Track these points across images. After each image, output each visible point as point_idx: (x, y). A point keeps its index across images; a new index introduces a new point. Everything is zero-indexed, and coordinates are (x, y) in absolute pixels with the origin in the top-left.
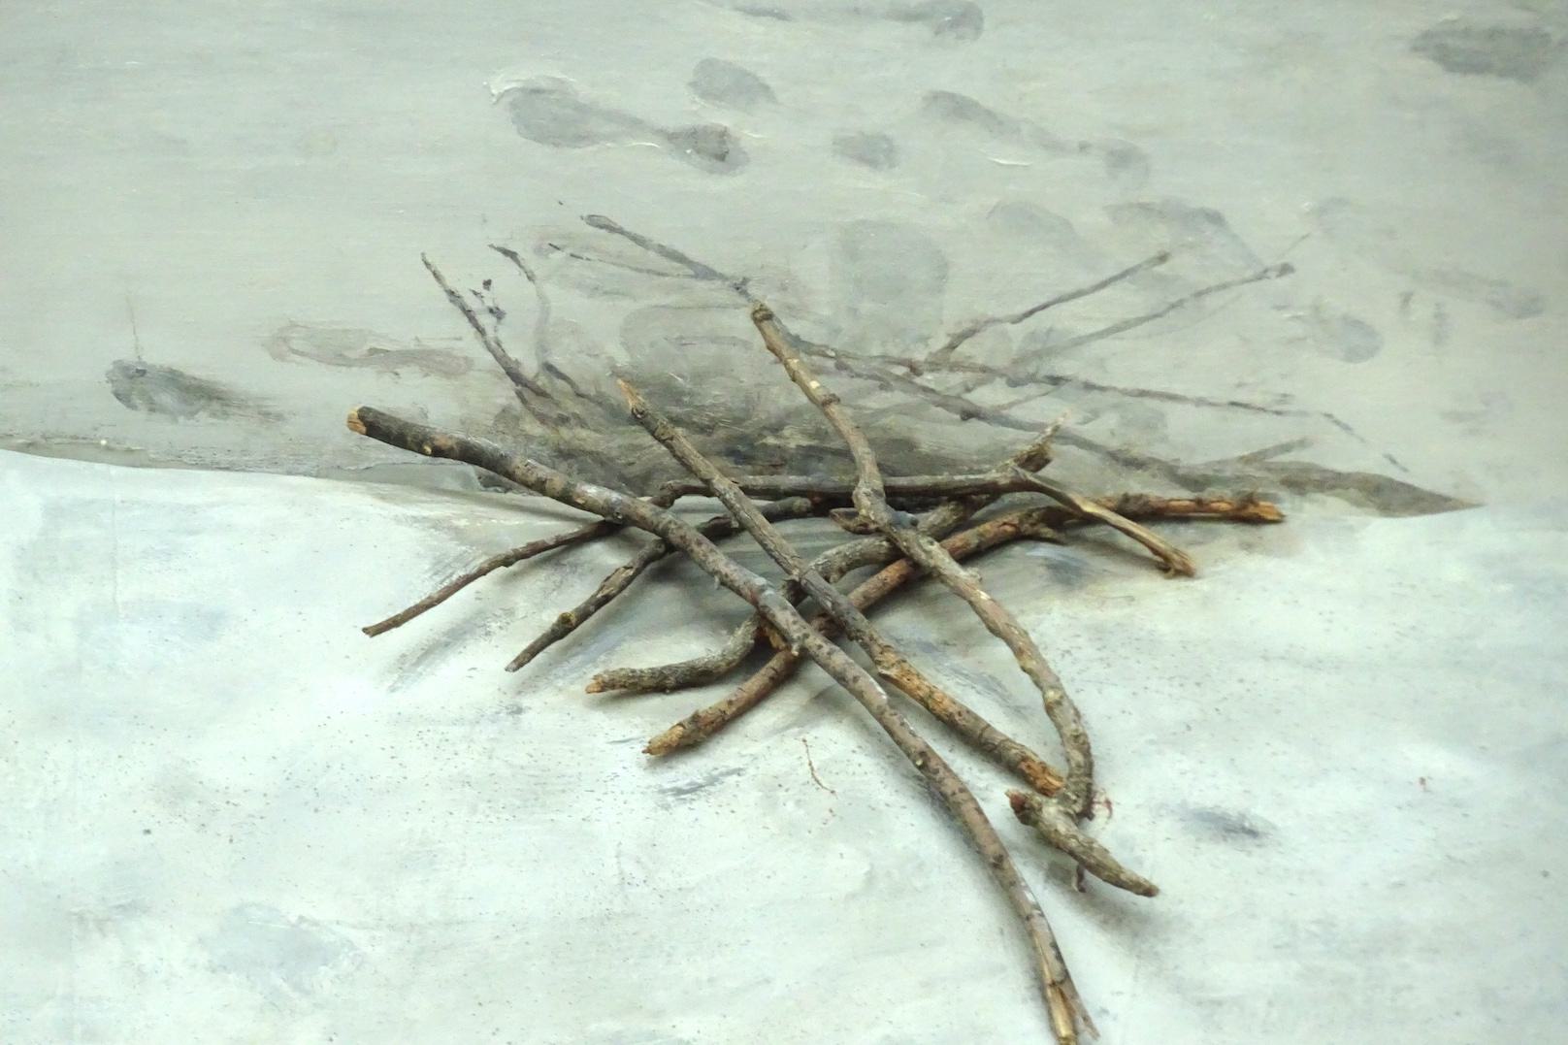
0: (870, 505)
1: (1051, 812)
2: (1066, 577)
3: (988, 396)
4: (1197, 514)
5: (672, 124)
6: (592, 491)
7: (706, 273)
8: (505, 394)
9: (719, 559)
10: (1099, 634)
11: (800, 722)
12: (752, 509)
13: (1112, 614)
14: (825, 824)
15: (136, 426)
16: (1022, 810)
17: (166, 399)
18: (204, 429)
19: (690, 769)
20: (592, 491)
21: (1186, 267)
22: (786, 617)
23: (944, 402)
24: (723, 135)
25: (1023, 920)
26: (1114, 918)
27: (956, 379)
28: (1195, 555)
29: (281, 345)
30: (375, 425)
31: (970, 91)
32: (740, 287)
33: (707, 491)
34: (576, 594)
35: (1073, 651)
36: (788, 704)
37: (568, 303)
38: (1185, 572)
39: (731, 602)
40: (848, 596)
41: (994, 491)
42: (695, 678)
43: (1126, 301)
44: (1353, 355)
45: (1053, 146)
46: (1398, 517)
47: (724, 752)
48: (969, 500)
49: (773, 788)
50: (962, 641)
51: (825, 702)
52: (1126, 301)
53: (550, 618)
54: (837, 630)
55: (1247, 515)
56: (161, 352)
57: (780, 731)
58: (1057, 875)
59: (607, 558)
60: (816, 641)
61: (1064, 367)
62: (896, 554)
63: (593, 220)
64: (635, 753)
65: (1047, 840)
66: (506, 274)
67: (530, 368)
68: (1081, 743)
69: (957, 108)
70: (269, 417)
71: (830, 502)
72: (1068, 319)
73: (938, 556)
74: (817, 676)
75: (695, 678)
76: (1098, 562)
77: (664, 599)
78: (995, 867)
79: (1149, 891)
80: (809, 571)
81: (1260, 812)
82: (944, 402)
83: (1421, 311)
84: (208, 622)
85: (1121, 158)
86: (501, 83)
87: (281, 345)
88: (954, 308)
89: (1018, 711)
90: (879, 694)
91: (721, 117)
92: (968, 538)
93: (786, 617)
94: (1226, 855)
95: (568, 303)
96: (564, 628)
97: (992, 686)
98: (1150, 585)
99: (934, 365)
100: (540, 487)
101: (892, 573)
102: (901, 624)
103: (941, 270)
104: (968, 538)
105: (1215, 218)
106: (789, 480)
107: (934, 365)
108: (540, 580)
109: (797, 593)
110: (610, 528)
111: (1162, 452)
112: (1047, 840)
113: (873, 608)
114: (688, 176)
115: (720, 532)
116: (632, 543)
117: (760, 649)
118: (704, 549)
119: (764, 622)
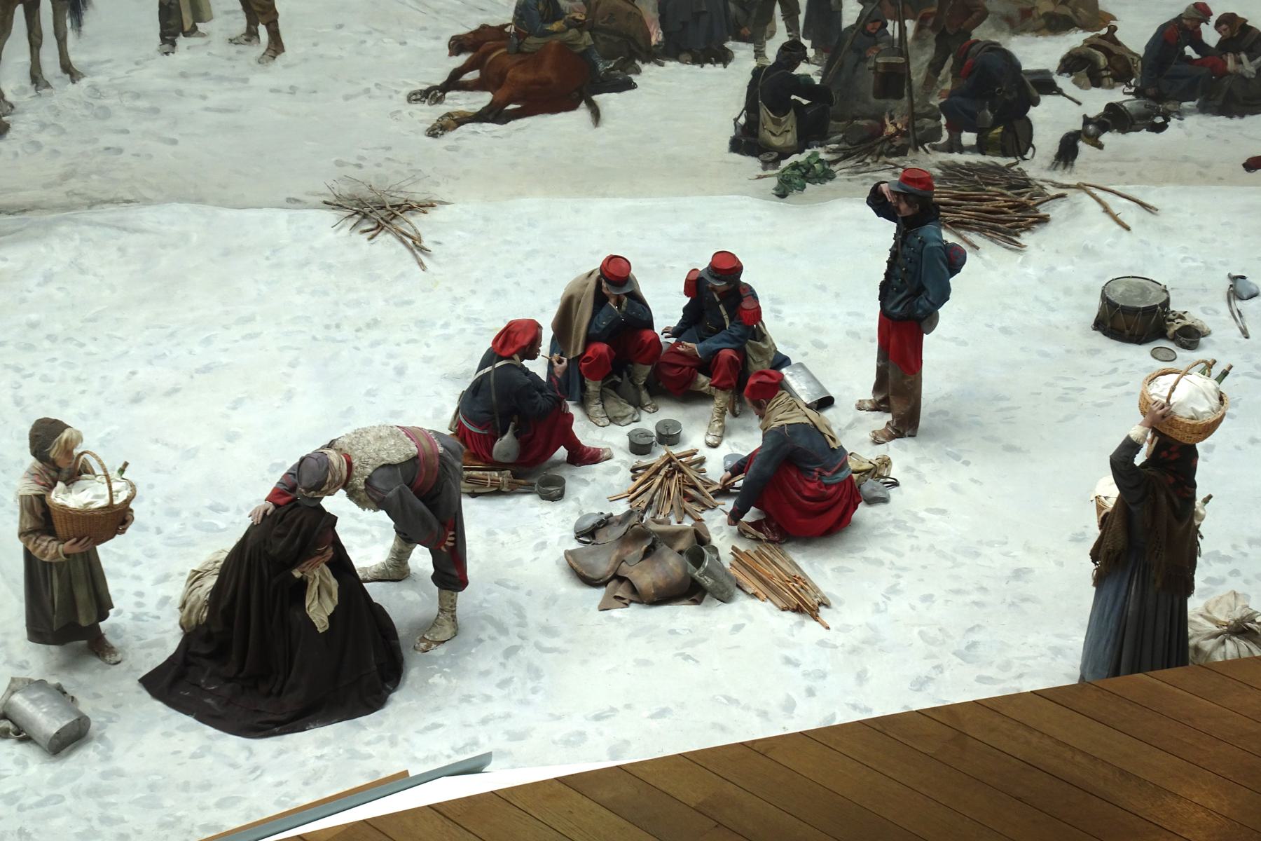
0: (388, 207)
1: (417, 243)
2: (413, 215)
3: (393, 194)
4: (427, 206)
5: (354, 163)
6: (355, 208)
7: (359, 181)
8: (335, 198)
9: (372, 215)
10: (418, 221)
11: (385, 234)
12: (375, 209)
13: (419, 219)
14: (104, 378)
15: (289, 205)
16: (414, 243)
17: (293, 201)
18: (297, 205)
19: (373, 241)
20: (355, 208)
21: (417, 177)
22: (382, 222)
23: (388, 195)
24: (360, 164)
25: (416, 256)
26: (426, 255)
27: (389, 192)
28: (428, 211)
29: (307, 194)
30: (325, 203)
31: (390, 157)
32: (363, 183)
33: (369, 207)
34: (355, 221)
35: (455, 125)
36: (383, 232)
37: (342, 186)
38: (426, 213)
39: (374, 220)
40: (388, 219)
41: (402, 205)
42: (372, 230)
43: (410, 181)
44: (437, 186)
45: (400, 163)
46: (1059, 34)
47: (376, 239)
48: (399, 206)
49: (383, 243)
50: (402, 223)
51: (387, 232)
52: (410, 181)
53: (353, 224)
54: (387, 222)
55: (432, 206)
56: (292, 196)
57: (382, 235)
58: (418, 250)
59: (357, 216)
60: (386, 224)
61: (403, 190)
62: (393, 213)
63: (345, 176)
64: (366, 239)
65: (416, 246)
66: (335, 183)
67: (338, 194)
68: (419, 234)
69: (389, 159)
70: (305, 203)
71: (383, 208)
72: (403, 184)
73: (398, 213)
74: (386, 228)
75: (372, 230)
76: (416, 212)
77: (365, 221)
78: (411, 250)
79: (430, 251)
80: (383, 216)
81: (441, 241)
82: (388, 195)
83: (445, 180)
84: (311, 228)
85: (409, 164)
86: (333, 159)
87: (307, 194)
88: (390, 183)
89: (410, 230)
90: (394, 230)
91: (361, 162)
92: (401, 211)
93: (382, 222)
94: (438, 246)
95: (342, 186)
96: (355, 225)
97: (406, 228)
98: (423, 215)
99: (388, 190)
100: (348, 208)
101: (392, 216)
102: (394, 222)
103: (387, 179)
104: (401, 211)
105: (420, 170)
106: (378, 205)
107: (388, 190)
108: (350, 219)
109: (382, 219)
110: (357, 213)
111: (414, 200)
112: (416, 246)
113: (391, 220)
114: (356, 170)
115: (371, 212)
116: (360, 215)
117: (378, 226)
118: (370, 214)
119: (378, 222)
